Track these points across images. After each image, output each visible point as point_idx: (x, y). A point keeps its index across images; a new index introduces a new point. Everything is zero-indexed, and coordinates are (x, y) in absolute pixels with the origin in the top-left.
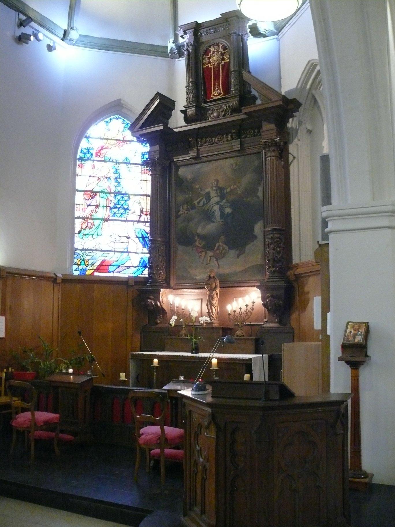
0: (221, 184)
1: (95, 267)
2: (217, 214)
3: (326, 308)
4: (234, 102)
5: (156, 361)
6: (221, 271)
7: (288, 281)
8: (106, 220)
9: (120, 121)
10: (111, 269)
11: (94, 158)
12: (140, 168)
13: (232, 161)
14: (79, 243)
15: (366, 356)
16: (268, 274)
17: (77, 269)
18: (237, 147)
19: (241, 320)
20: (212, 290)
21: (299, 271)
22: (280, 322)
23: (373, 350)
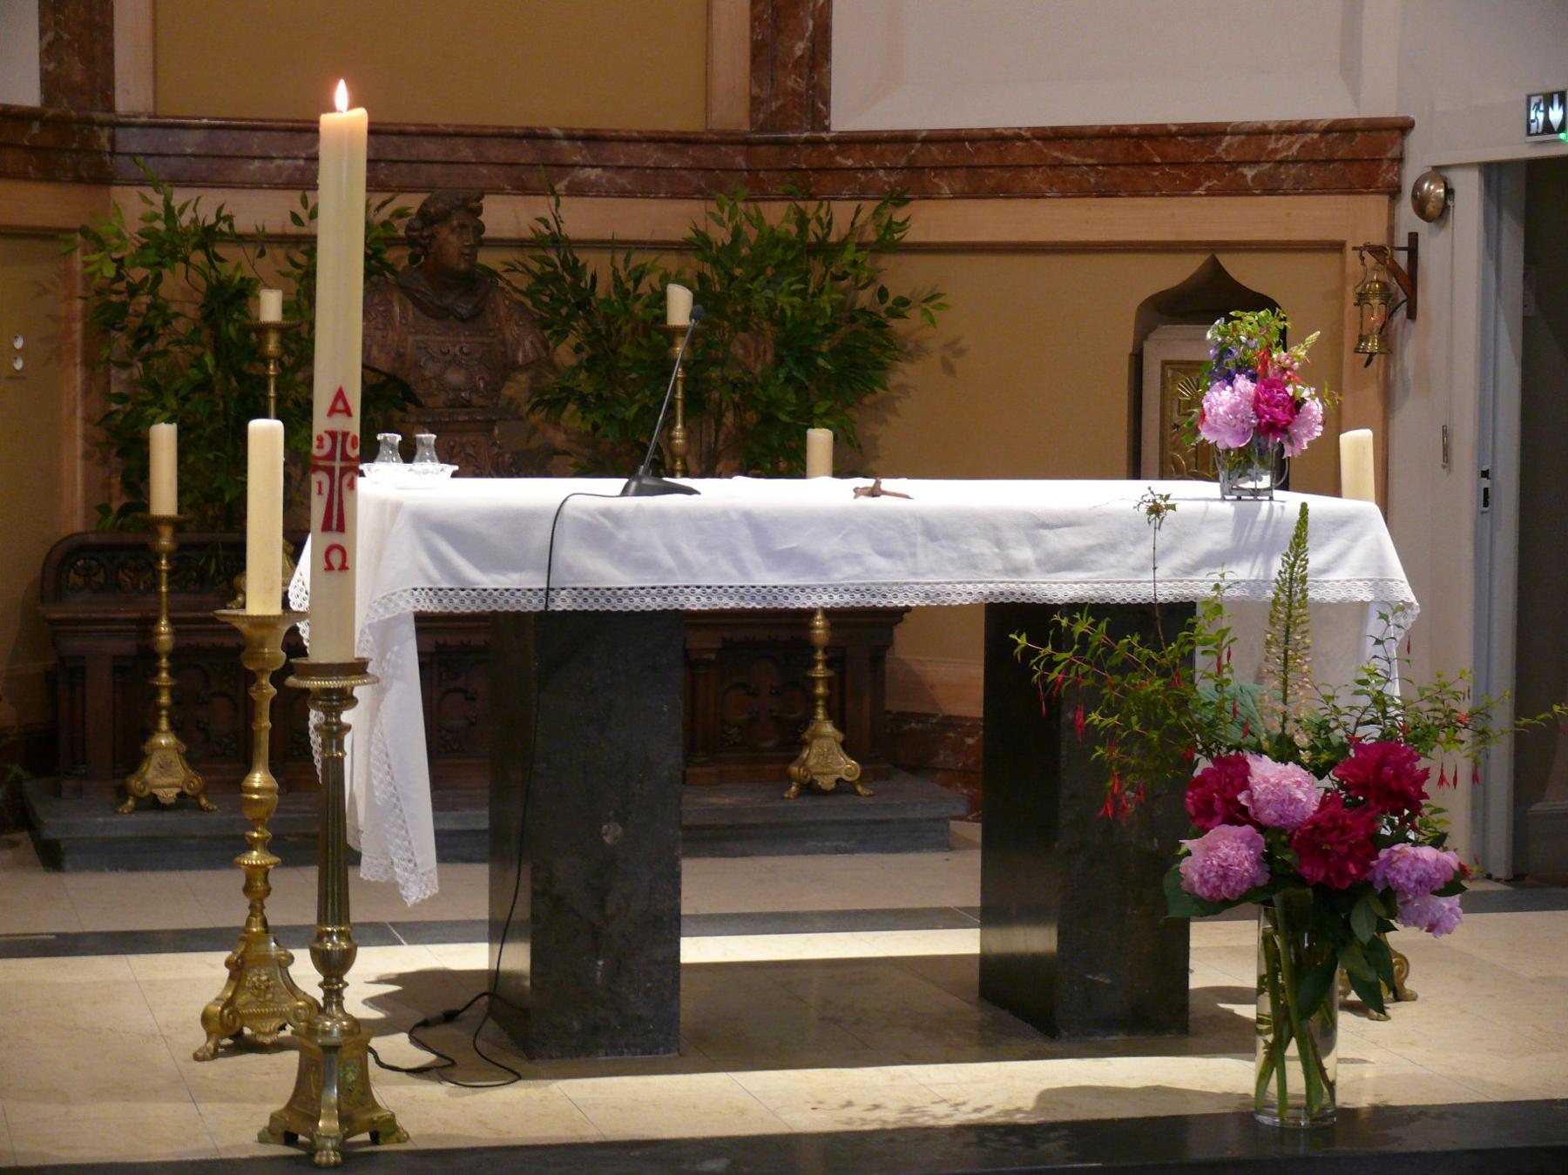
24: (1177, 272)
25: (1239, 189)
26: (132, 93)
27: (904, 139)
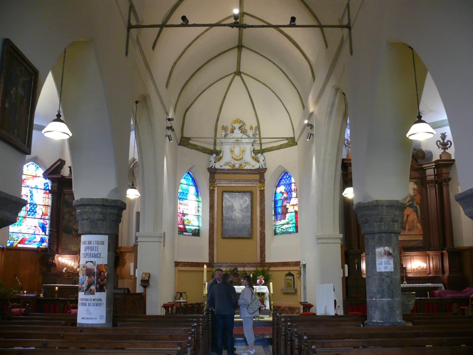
1: (18, 242)
3: (135, 267)
5: (57, 288)
8: (25, 217)
9: (34, 166)
10: (26, 242)
12: (43, 191)
17: (9, 243)
21: (122, 250)
23: (151, 282)
24: (287, 272)
25: (290, 266)
26: (215, 261)
27: (269, 263)
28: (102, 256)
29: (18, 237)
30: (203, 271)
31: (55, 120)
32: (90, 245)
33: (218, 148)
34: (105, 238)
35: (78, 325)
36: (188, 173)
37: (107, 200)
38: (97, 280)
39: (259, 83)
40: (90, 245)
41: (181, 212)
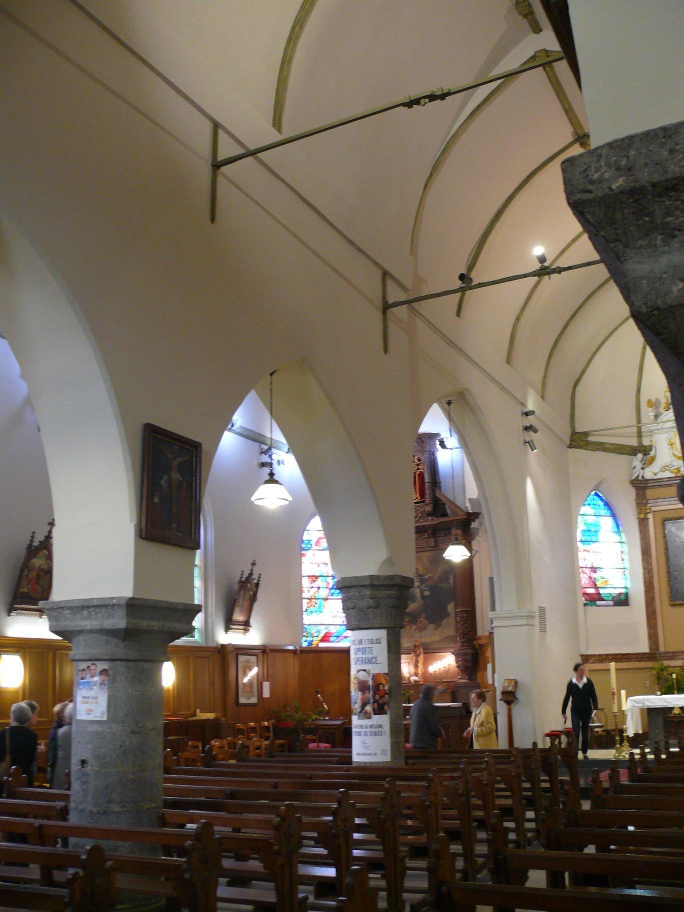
0: (421, 572)
1: (319, 638)
2: (419, 596)
3: (494, 672)
4: (429, 509)
6: (423, 640)
7: (474, 648)
8: (326, 599)
10: (332, 639)
11: (314, 547)
13: (429, 554)
14: (307, 619)
15: (515, 697)
16: (459, 644)
18: (433, 544)
19: (439, 678)
20: (417, 656)
22: (469, 679)
23: (520, 695)
26: (662, 649)
28: (379, 660)
29: (318, 631)
30: (609, 670)
31: (267, 482)
32: (361, 646)
33: (646, 442)
34: (382, 634)
35: (354, 765)
36: (596, 494)
37: (378, 577)
38: (374, 698)
39: (594, 361)
40: (361, 646)
41: (590, 566)
